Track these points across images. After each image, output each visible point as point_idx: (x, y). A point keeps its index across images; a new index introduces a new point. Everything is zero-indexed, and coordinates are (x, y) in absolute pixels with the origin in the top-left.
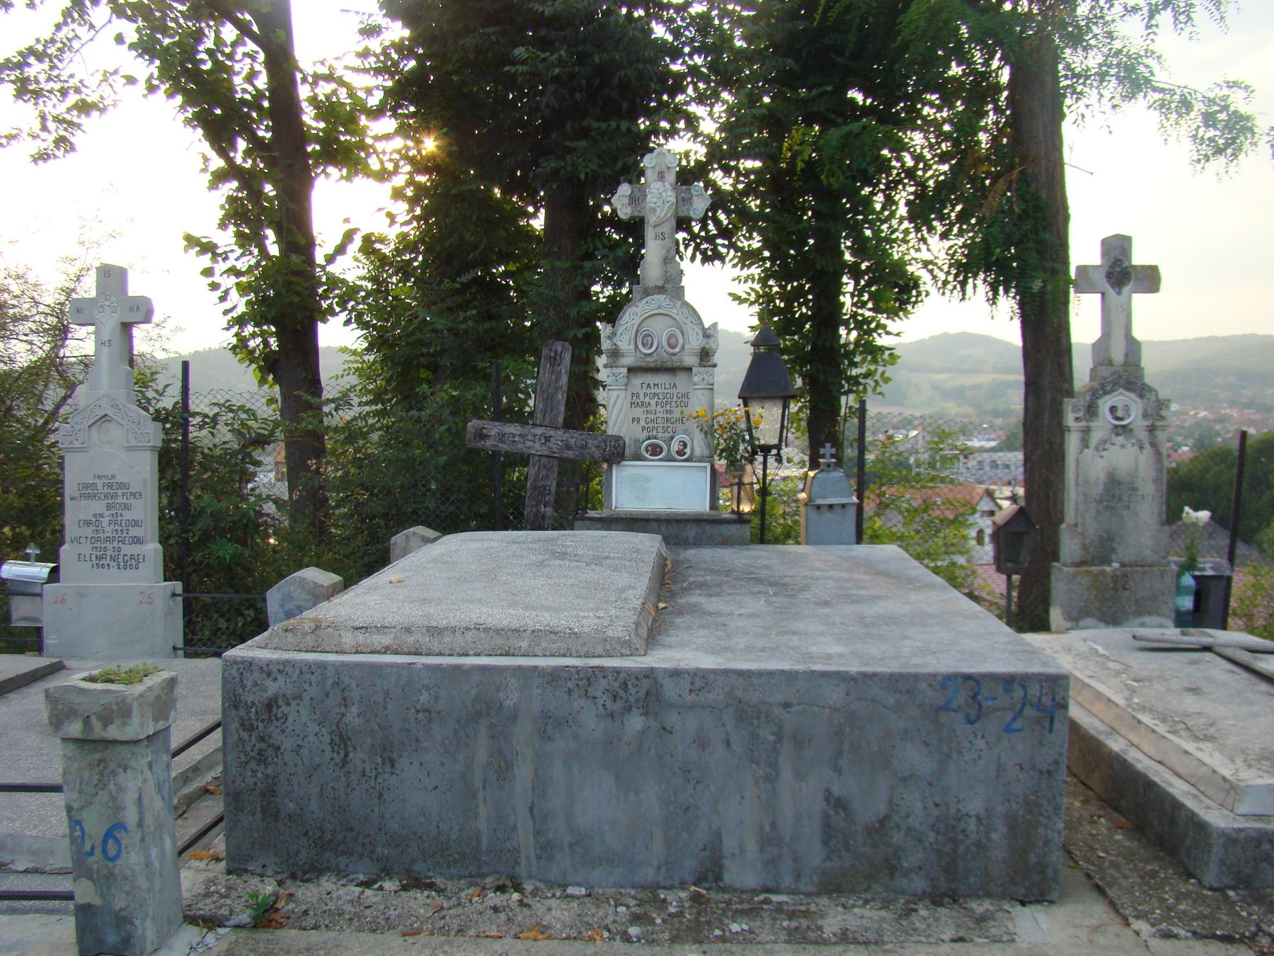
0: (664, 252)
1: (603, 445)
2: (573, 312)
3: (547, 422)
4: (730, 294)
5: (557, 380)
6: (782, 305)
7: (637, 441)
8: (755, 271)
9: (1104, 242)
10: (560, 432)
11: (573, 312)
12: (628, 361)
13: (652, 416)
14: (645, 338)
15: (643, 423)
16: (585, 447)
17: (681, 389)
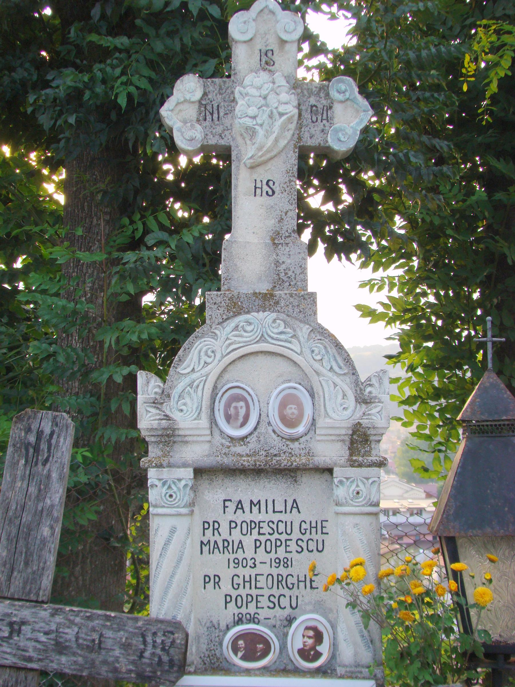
0: (272, 223)
1: (137, 642)
2: (109, 339)
3: (16, 586)
4: (359, 307)
5: (40, 496)
6: (439, 323)
7: (213, 626)
8: (395, 272)
9: (316, 293)
10: (44, 613)
11: (109, 339)
12: (196, 452)
13: (247, 572)
14: (230, 402)
15: (226, 587)
16: (97, 646)
17: (309, 513)
